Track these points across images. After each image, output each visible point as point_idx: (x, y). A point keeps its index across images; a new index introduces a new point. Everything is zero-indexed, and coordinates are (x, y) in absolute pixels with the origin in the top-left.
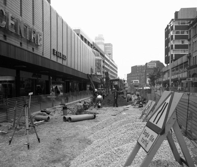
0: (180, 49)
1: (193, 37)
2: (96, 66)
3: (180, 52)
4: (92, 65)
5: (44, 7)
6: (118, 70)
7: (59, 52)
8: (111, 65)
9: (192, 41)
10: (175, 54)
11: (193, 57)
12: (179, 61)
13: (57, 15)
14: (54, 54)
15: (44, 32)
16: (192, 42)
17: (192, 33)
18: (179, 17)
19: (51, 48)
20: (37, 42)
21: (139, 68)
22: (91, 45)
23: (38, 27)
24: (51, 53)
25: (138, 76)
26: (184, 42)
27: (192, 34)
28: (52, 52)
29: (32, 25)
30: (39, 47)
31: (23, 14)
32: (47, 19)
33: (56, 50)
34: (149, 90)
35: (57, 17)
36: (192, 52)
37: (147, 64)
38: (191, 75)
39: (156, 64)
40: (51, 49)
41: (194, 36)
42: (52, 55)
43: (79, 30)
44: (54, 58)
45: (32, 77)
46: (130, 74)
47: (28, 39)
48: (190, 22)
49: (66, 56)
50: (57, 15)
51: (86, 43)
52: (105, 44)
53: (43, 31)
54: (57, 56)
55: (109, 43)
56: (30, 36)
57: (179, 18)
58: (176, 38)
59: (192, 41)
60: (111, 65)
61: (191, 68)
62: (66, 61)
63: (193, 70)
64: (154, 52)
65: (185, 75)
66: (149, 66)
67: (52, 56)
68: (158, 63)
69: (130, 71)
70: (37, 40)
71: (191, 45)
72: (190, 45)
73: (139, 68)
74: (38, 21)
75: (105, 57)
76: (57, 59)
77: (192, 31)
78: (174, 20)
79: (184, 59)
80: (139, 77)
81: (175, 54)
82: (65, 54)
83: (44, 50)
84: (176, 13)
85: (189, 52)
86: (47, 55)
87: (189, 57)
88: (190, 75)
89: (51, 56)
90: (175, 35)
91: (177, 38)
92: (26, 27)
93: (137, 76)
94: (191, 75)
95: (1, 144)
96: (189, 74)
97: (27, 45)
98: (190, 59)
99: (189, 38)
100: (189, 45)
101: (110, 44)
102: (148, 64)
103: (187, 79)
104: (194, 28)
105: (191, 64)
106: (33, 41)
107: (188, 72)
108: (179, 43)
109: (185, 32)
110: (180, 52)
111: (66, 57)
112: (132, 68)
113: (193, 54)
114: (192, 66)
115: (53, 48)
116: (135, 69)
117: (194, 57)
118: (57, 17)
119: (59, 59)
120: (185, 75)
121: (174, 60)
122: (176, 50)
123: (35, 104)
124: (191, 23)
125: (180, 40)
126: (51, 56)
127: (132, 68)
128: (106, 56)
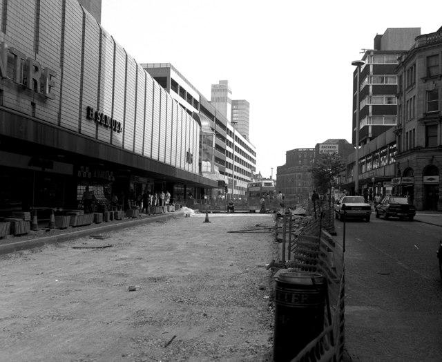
2: (200, 146)
3: (383, 122)
5: (66, 13)
7: (102, 114)
8: (236, 144)
10: (373, 126)
12: (379, 141)
13: (101, 33)
14: (88, 118)
15: (65, 69)
16: (405, 100)
17: (405, 80)
19: (81, 104)
21: (303, 155)
22: (196, 102)
23: (48, 58)
24: (80, 115)
26: (393, 100)
28: (84, 113)
29: (33, 53)
30: (49, 102)
31: (8, 28)
32: (92, 46)
33: (96, 109)
34: (403, 206)
35: (101, 37)
39: (337, 146)
40: (81, 108)
42: (84, 120)
43: (167, 69)
44: (89, 128)
45: (30, 165)
46: (284, 166)
47: (18, 81)
48: (400, 59)
49: (122, 123)
50: (101, 33)
51: (184, 98)
53: (62, 66)
54: (98, 124)
57: (383, 49)
58: (374, 93)
60: (236, 144)
61: (401, 154)
64: (330, 120)
67: (82, 121)
68: (342, 142)
69: (282, 161)
70: (43, 86)
72: (400, 106)
73: (303, 155)
76: (97, 129)
78: (372, 53)
79: (389, 136)
80: (301, 174)
81: (373, 126)
82: (118, 118)
83: (62, 108)
84: (378, 39)
85: (399, 121)
87: (399, 131)
88: (399, 171)
89: (80, 122)
90: (373, 86)
91: (378, 90)
92: (15, 56)
93: (298, 172)
95: (3, 296)
97: (18, 96)
99: (398, 92)
100: (398, 108)
102: (321, 146)
105: (402, 146)
106: (31, 86)
108: (382, 101)
110: (383, 122)
111: (122, 126)
112: (289, 153)
114: (404, 152)
115: (87, 105)
116: (292, 155)
118: (101, 37)
119: (101, 129)
120: (390, 171)
124: (403, 60)
125: (384, 96)
126: (80, 122)
127: (289, 153)
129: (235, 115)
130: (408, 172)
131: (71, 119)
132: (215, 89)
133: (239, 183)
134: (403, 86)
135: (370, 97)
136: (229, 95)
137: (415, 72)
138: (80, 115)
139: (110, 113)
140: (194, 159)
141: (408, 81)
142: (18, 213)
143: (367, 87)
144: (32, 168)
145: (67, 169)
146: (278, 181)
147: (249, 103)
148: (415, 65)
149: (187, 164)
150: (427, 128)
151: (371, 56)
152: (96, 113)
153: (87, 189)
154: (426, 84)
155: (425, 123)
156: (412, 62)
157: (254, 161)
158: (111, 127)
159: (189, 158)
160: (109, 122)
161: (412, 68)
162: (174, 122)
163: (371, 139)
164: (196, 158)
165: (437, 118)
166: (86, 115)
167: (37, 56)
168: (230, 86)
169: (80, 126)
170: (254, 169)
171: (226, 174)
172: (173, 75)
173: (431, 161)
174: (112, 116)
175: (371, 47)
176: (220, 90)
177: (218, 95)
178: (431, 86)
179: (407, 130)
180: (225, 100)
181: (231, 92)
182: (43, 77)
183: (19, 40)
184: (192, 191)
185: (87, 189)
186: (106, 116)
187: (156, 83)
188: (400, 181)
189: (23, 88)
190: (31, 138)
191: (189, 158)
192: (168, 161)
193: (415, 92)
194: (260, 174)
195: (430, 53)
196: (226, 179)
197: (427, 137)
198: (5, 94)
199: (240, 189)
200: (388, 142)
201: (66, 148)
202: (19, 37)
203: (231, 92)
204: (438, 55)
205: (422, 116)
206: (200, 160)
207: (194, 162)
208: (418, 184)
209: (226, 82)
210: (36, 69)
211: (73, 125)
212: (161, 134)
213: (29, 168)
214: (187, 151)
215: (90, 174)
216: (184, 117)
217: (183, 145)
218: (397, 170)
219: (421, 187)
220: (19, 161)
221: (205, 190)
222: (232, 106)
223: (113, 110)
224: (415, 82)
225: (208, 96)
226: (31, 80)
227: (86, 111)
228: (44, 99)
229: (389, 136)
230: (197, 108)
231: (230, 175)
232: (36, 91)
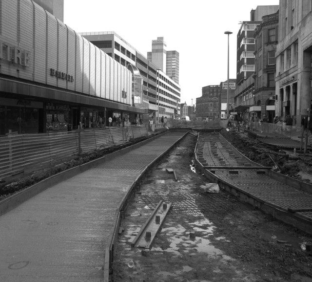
2: (133, 87)
4: (125, 86)
13: (58, 24)
19: (46, 67)
20: (23, 63)
21: (213, 90)
22: (133, 56)
23: (25, 44)
24: (46, 74)
25: (211, 101)
30: (27, 68)
37: (222, 83)
39: (235, 84)
40: (46, 69)
42: (49, 77)
44: (52, 81)
47: (9, 60)
50: (58, 24)
52: (167, 52)
56: (13, 56)
57: (255, 21)
58: (248, 49)
62: (74, 83)
69: (200, 95)
70: (23, 60)
74: (24, 39)
80: (212, 103)
84: (253, 13)
86: (40, 77)
89: (46, 78)
106: (16, 61)
111: (74, 78)
115: (51, 68)
119: (59, 80)
123: (37, 145)
126: (46, 78)
127: (205, 90)
129: (168, 62)
131: (41, 76)
132: (154, 43)
133: (167, 110)
135: (246, 53)
136: (164, 48)
138: (46, 74)
139: (66, 71)
140: (128, 95)
142: (235, 170)
143: (243, 45)
144: (18, 105)
145: (40, 105)
146: (197, 108)
150: (268, 74)
151: (246, 25)
152: (56, 71)
153: (53, 116)
157: (179, 95)
158: (66, 79)
159: (124, 95)
160: (65, 76)
162: (112, 71)
163: (246, 80)
164: (130, 94)
166: (50, 73)
167: (19, 44)
168: (165, 41)
169: (46, 80)
170: (179, 100)
171: (157, 104)
172: (116, 39)
174: (67, 73)
175: (249, 19)
177: (157, 47)
180: (161, 51)
181: (166, 46)
182: (23, 55)
183: (9, 37)
185: (53, 116)
186: (62, 73)
189: (12, 63)
190: (15, 91)
191: (124, 95)
192: (107, 97)
194: (185, 103)
195: (270, 27)
197: (269, 81)
198: (2, 67)
199: (168, 114)
201: (34, 95)
202: (9, 35)
203: (166, 46)
206: (133, 95)
207: (128, 97)
209: (162, 38)
210: (19, 51)
211: (42, 80)
212: (107, 80)
213: (17, 106)
214: (122, 90)
215: (54, 107)
217: (119, 84)
220: (13, 103)
221: (138, 115)
222: (167, 54)
226: (16, 59)
227: (50, 71)
228: (24, 67)
231: (160, 104)
232: (19, 64)
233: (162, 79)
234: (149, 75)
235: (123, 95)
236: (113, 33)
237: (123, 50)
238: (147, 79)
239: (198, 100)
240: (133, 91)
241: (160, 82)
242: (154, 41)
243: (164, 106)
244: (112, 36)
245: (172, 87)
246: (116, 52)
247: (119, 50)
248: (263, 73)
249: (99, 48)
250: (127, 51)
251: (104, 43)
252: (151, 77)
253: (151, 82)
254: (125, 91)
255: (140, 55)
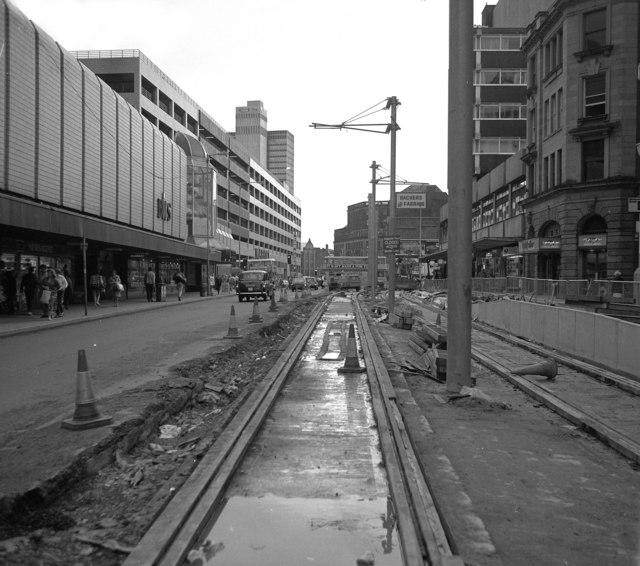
0: (499, 139)
1: (544, 81)
2: (190, 192)
6: (303, 218)
9: (541, 94)
10: (481, 156)
11: (544, 156)
12: (495, 179)
16: (541, 99)
17: (541, 64)
18: (498, 24)
22: (192, 122)
27: (541, 68)
36: (541, 140)
38: (537, 229)
39: (424, 196)
41: (548, 77)
55: (292, 133)
59: (541, 94)
61: (535, 199)
63: (543, 206)
65: (514, 229)
66: (401, 204)
68: (431, 190)
69: (343, 223)
71: (538, 112)
75: (252, 170)
77: (541, 58)
79: (513, 168)
88: (532, 229)
94: (537, 229)
96: (404, 442)
98: (532, 167)
101: (285, 132)
103: (520, 244)
104: (548, 46)
107: (524, 218)
109: (516, 76)
112: (351, 209)
113: (546, 145)
117: (547, 158)
120: (514, 229)
121: (479, 177)
122: (484, 139)
124: (538, 27)
127: (336, 231)
128: (253, 164)
130: (548, 229)
132: (241, 113)
134: (538, 77)
137: (561, 45)
140: (175, 212)
141: (592, 135)
147: (293, 136)
148: (560, 32)
149: (160, 221)
154: (583, 65)
155: (581, 137)
156: (554, 29)
161: (554, 40)
165: (603, 127)
168: (268, 108)
171: (251, 241)
173: (593, 207)
176: (253, 116)
177: (247, 122)
178: (592, 67)
179: (547, 153)
184: (192, 273)
187: (106, 87)
188: (535, 245)
193: (562, 82)
196: (247, 250)
200: (509, 179)
204: (605, 9)
205: (574, 125)
208: (569, 251)
216: (148, 137)
218: (528, 226)
219: (574, 254)
223: (101, 153)
224: (561, 65)
225: (227, 123)
229: (513, 168)
230: (195, 132)
231: (257, 243)
233: (267, 188)
234: (231, 173)
235: (160, 211)
236: (136, 56)
237: (165, 102)
238: (225, 182)
239: (339, 235)
240: (189, 203)
241: (257, 191)
242: (239, 110)
243: (266, 246)
244: (134, 61)
245: (263, 190)
246: (145, 102)
247: (153, 100)
248: (568, 142)
249: (113, 88)
250: (176, 106)
251: (122, 75)
252: (238, 180)
253: (235, 189)
254: (167, 199)
255: (209, 121)
